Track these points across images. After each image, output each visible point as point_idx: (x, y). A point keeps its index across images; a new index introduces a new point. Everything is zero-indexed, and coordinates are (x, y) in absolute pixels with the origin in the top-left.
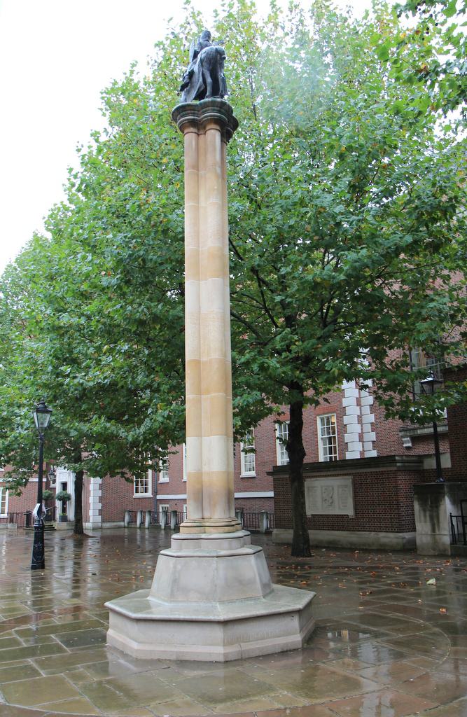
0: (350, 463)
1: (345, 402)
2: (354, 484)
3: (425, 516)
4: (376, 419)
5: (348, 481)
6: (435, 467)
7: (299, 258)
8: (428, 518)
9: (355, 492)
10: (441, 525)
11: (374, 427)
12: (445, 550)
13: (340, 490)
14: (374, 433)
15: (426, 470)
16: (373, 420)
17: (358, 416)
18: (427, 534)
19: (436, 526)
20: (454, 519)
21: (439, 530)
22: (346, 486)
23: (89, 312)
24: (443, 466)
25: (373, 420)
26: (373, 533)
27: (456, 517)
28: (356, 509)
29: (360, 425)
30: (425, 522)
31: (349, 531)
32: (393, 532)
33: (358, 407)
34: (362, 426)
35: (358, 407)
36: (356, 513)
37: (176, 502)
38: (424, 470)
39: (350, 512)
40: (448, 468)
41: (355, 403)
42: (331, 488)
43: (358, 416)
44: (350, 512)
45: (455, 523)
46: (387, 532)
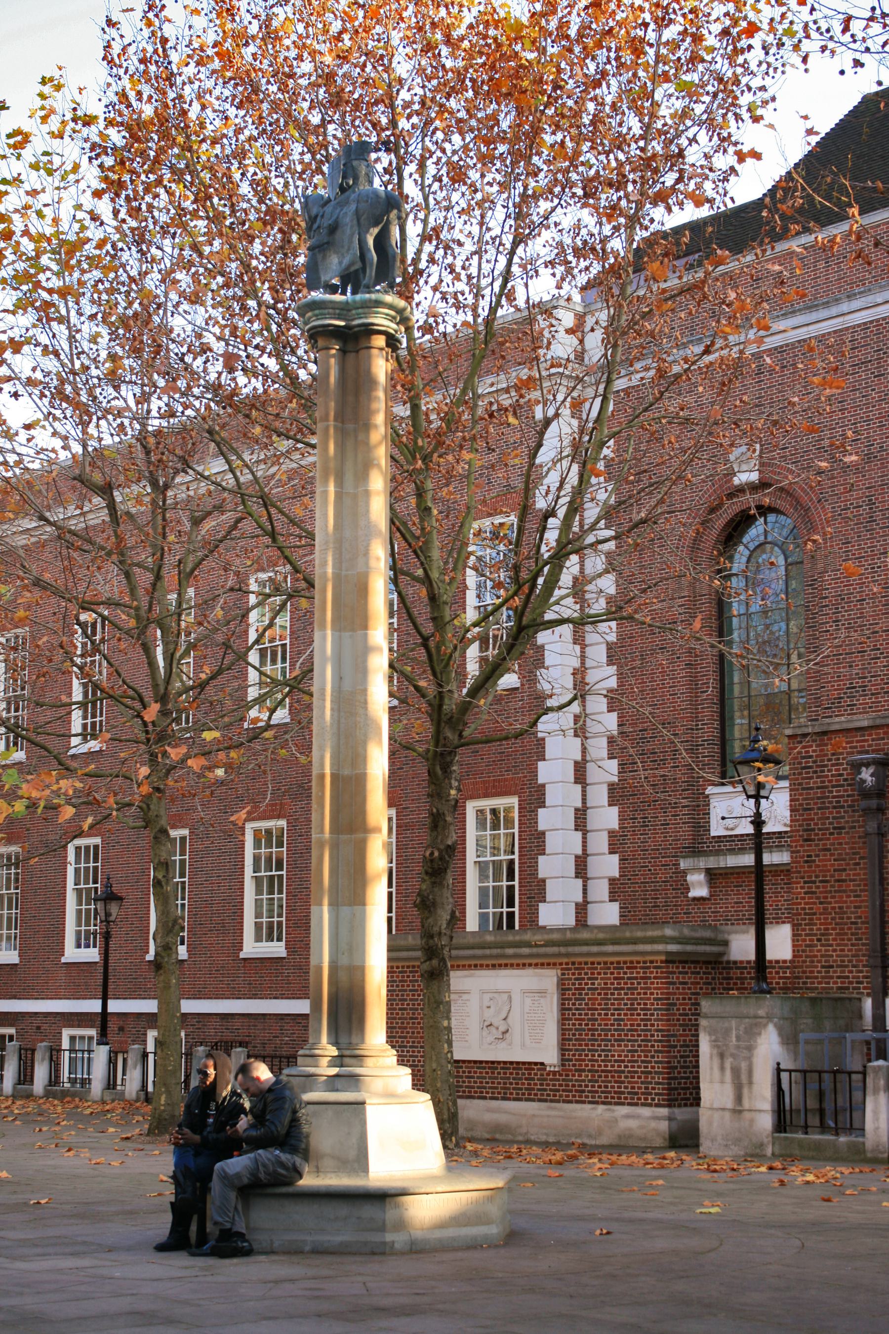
0: (555, 936)
1: (545, 772)
2: (562, 988)
3: (722, 1068)
4: (622, 819)
5: (541, 923)
6: (751, 955)
7: (98, 252)
8: (728, 1073)
9: (563, 1009)
10: (755, 1087)
11: (616, 843)
12: (761, 1145)
13: (528, 1001)
14: (615, 858)
15: (735, 962)
16: (613, 683)
17: (577, 810)
18: (723, 1109)
19: (745, 1091)
20: (785, 1076)
21: (750, 1098)
22: (542, 993)
23: (755, 56)
24: (771, 954)
25: (615, 825)
26: (601, 1108)
27: (790, 1071)
28: (563, 1049)
29: (579, 834)
30: (722, 1082)
31: (545, 1101)
32: (650, 1105)
33: (579, 787)
34: (583, 652)
35: (579, 787)
36: (563, 1060)
37: (37, 1022)
38: (728, 962)
39: (550, 1056)
40: (785, 961)
41: (570, 773)
42: (505, 996)
43: (577, 810)
44: (550, 1056)
45: (785, 1086)
46: (636, 1104)
